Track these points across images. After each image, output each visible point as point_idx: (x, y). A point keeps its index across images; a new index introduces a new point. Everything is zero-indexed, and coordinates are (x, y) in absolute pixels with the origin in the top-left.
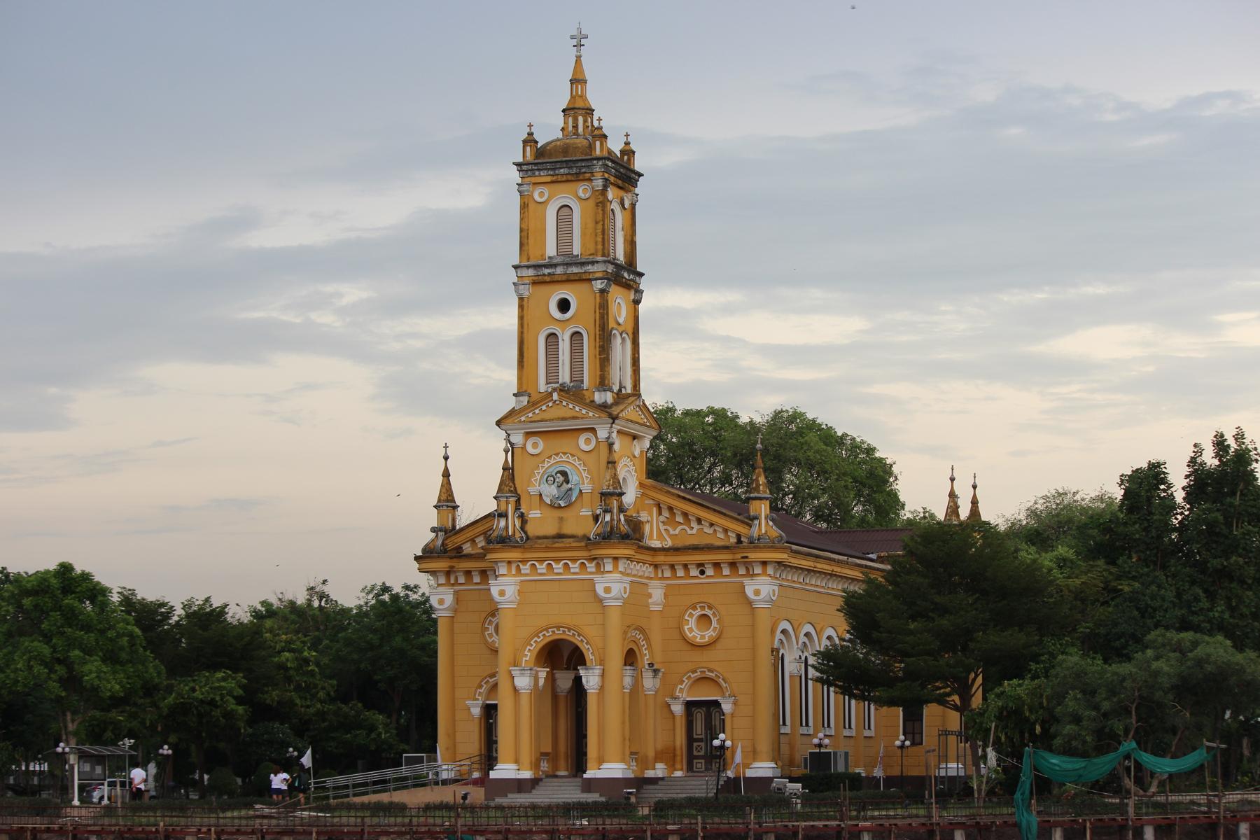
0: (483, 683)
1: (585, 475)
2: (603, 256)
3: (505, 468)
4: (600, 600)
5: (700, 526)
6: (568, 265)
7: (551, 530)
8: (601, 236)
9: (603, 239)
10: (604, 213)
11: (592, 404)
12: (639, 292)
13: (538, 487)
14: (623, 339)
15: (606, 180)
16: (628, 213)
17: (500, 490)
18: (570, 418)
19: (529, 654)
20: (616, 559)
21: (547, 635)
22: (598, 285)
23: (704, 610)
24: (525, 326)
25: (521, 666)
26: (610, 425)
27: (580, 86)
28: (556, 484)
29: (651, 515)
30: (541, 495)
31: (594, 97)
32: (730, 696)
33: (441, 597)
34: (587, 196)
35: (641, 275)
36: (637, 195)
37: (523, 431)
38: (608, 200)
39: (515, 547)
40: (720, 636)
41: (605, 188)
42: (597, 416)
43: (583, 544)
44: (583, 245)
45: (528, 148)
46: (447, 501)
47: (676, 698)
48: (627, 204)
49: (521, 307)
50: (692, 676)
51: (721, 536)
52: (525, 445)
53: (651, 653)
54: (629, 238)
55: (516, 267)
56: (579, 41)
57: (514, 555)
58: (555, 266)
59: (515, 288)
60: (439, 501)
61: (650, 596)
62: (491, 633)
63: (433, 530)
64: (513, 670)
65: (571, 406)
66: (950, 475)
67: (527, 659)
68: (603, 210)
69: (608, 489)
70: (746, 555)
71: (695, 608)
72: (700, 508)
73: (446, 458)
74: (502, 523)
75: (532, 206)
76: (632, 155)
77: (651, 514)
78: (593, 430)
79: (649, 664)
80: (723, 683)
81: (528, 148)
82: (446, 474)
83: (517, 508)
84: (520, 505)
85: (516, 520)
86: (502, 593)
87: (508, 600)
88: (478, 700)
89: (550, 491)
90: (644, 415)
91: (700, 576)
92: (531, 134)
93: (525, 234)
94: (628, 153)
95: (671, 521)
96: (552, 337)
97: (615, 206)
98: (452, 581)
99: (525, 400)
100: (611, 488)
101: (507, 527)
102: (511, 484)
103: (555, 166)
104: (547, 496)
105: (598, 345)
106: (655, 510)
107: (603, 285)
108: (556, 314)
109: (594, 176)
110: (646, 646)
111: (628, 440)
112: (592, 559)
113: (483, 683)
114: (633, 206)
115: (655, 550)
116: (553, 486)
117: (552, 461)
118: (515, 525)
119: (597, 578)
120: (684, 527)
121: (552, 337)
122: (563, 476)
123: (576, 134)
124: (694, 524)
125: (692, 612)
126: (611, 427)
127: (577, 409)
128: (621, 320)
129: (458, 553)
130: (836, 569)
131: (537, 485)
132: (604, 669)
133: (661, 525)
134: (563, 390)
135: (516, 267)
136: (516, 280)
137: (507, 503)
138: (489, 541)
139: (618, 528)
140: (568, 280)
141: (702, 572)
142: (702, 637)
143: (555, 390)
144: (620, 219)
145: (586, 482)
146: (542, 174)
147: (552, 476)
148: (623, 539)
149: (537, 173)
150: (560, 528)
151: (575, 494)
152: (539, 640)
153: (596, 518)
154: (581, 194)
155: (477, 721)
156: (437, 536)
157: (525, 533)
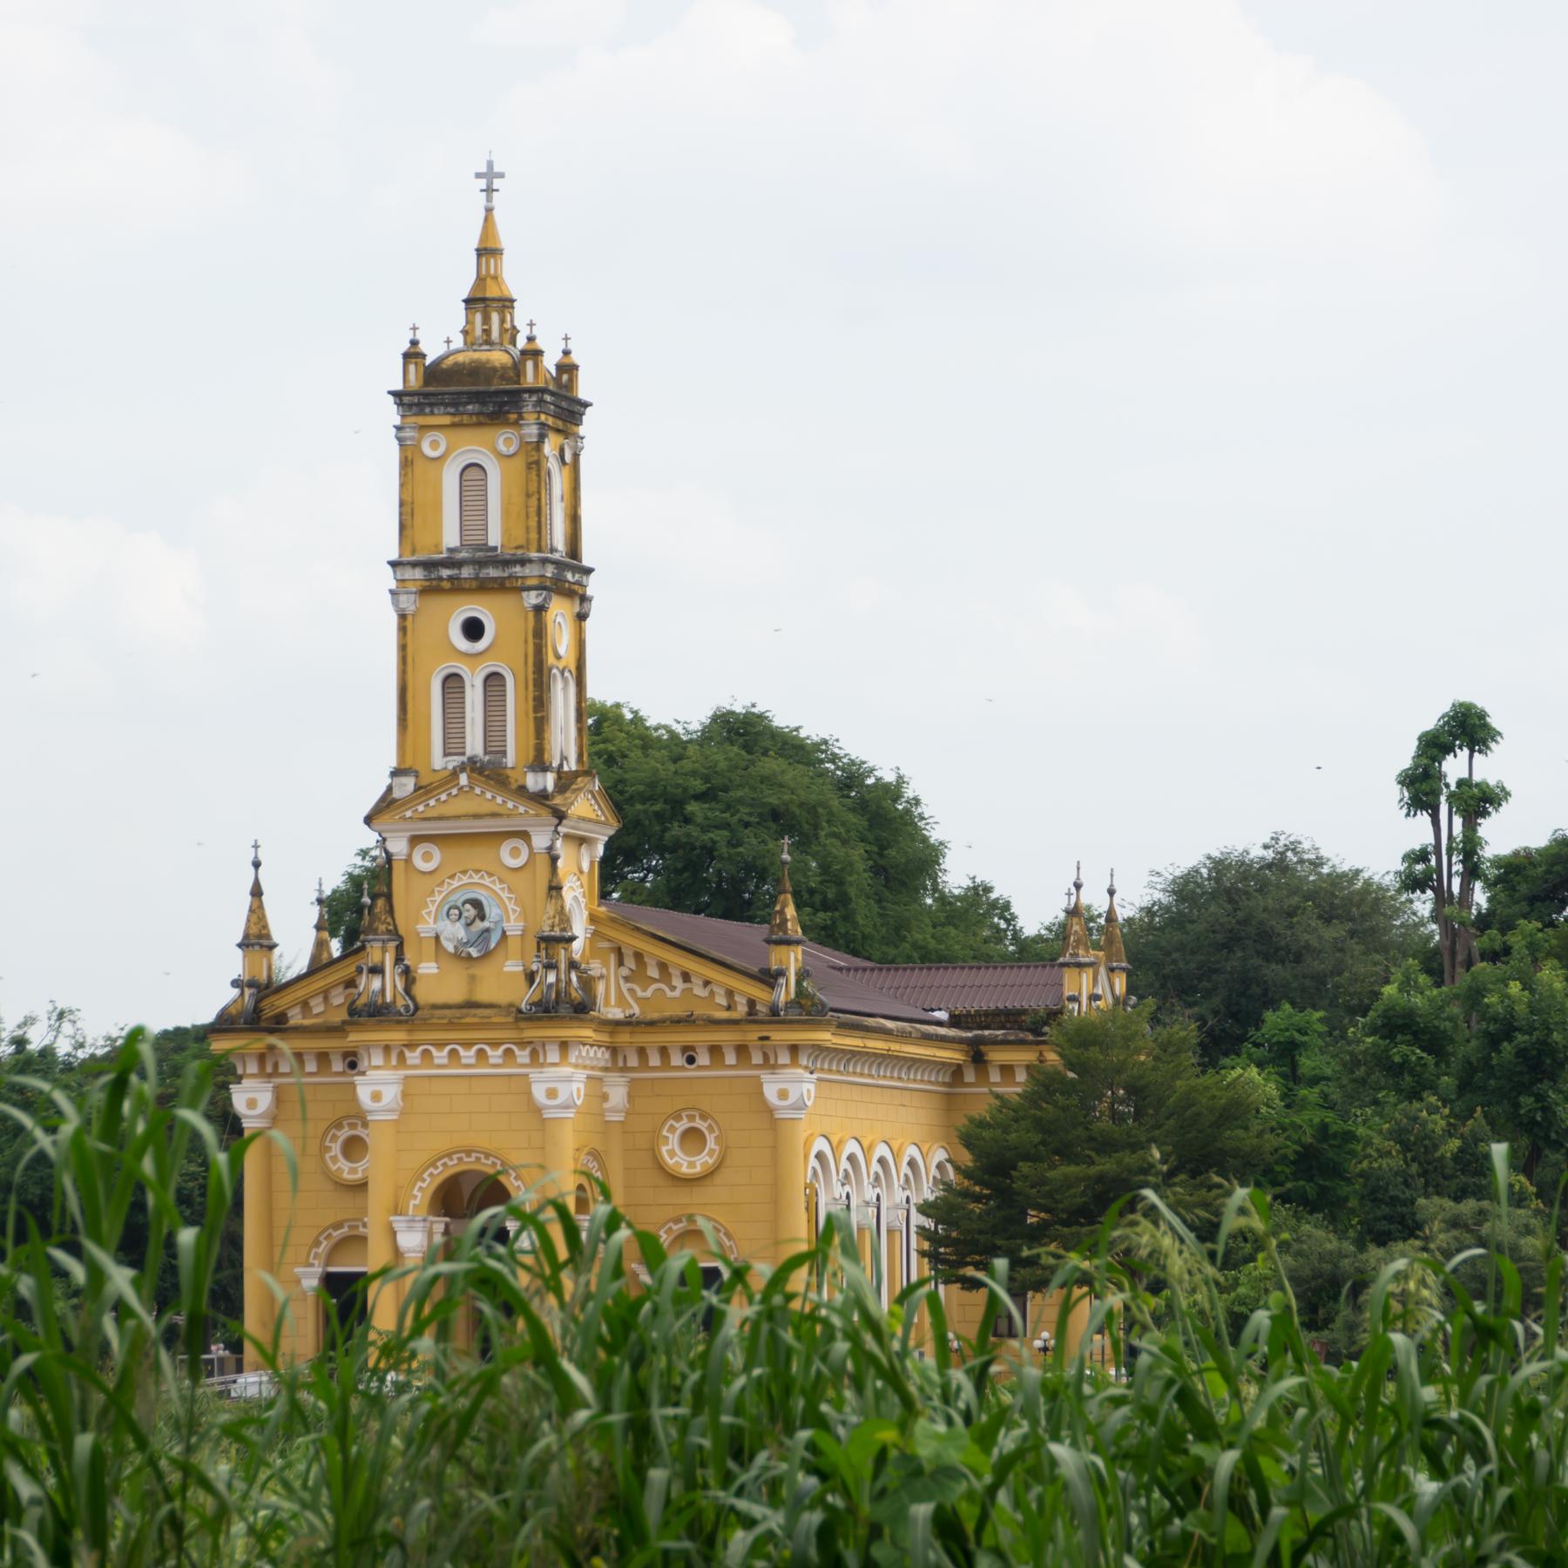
0: (321, 1238)
1: (511, 906)
2: (539, 550)
4: (537, 1110)
5: (688, 985)
6: (480, 564)
9: (539, 522)
10: (539, 476)
12: (584, 599)
13: (432, 925)
14: (565, 688)
15: (542, 425)
18: (487, 815)
19: (419, 1195)
20: (564, 1046)
22: (532, 598)
24: (409, 661)
25: (406, 1215)
27: (492, 261)
29: (608, 970)
30: (437, 938)
31: (514, 277)
33: (251, 1095)
34: (512, 450)
35: (589, 571)
37: (408, 834)
39: (399, 1022)
40: (721, 1162)
42: (531, 812)
43: (510, 1019)
44: (506, 531)
45: (412, 368)
46: (257, 940)
48: (568, 457)
49: (403, 630)
50: (675, 1227)
51: (722, 1000)
55: (394, 564)
57: (397, 1036)
58: (458, 564)
59: (393, 599)
60: (246, 936)
61: (605, 1097)
62: (336, 1156)
63: (236, 983)
65: (489, 795)
66: (1073, 879)
67: (417, 1202)
68: (539, 476)
71: (678, 1118)
72: (721, 969)
73: (257, 865)
74: (376, 984)
75: (419, 465)
77: (605, 964)
78: (524, 836)
81: (412, 368)
82: (257, 892)
83: (399, 959)
84: (402, 954)
85: (397, 978)
86: (376, 1097)
88: (312, 1265)
89: (453, 932)
92: (414, 343)
93: (407, 509)
94: (568, 369)
95: (638, 976)
96: (453, 683)
97: (553, 464)
98: (269, 1069)
101: (383, 990)
102: (389, 920)
103: (455, 403)
104: (448, 939)
105: (531, 696)
106: (613, 959)
108: (462, 643)
109: (522, 419)
112: (522, 1044)
113: (321, 1238)
114: (576, 456)
115: (617, 1023)
116: (458, 924)
117: (456, 883)
118: (395, 986)
119: (534, 1074)
120: (662, 986)
121: (453, 683)
123: (488, 342)
124: (677, 981)
127: (499, 800)
129: (279, 1024)
130: (895, 1047)
131: (431, 921)
133: (622, 982)
134: (473, 766)
135: (394, 564)
136: (393, 585)
137: (384, 950)
139: (567, 993)
140: (484, 587)
141: (691, 1060)
142: (691, 1165)
144: (559, 483)
145: (512, 917)
146: (436, 411)
147: (457, 908)
148: (576, 1012)
149: (427, 410)
151: (495, 938)
153: (530, 977)
154: (502, 448)
155: (311, 1302)
156: (242, 994)
157: (412, 998)
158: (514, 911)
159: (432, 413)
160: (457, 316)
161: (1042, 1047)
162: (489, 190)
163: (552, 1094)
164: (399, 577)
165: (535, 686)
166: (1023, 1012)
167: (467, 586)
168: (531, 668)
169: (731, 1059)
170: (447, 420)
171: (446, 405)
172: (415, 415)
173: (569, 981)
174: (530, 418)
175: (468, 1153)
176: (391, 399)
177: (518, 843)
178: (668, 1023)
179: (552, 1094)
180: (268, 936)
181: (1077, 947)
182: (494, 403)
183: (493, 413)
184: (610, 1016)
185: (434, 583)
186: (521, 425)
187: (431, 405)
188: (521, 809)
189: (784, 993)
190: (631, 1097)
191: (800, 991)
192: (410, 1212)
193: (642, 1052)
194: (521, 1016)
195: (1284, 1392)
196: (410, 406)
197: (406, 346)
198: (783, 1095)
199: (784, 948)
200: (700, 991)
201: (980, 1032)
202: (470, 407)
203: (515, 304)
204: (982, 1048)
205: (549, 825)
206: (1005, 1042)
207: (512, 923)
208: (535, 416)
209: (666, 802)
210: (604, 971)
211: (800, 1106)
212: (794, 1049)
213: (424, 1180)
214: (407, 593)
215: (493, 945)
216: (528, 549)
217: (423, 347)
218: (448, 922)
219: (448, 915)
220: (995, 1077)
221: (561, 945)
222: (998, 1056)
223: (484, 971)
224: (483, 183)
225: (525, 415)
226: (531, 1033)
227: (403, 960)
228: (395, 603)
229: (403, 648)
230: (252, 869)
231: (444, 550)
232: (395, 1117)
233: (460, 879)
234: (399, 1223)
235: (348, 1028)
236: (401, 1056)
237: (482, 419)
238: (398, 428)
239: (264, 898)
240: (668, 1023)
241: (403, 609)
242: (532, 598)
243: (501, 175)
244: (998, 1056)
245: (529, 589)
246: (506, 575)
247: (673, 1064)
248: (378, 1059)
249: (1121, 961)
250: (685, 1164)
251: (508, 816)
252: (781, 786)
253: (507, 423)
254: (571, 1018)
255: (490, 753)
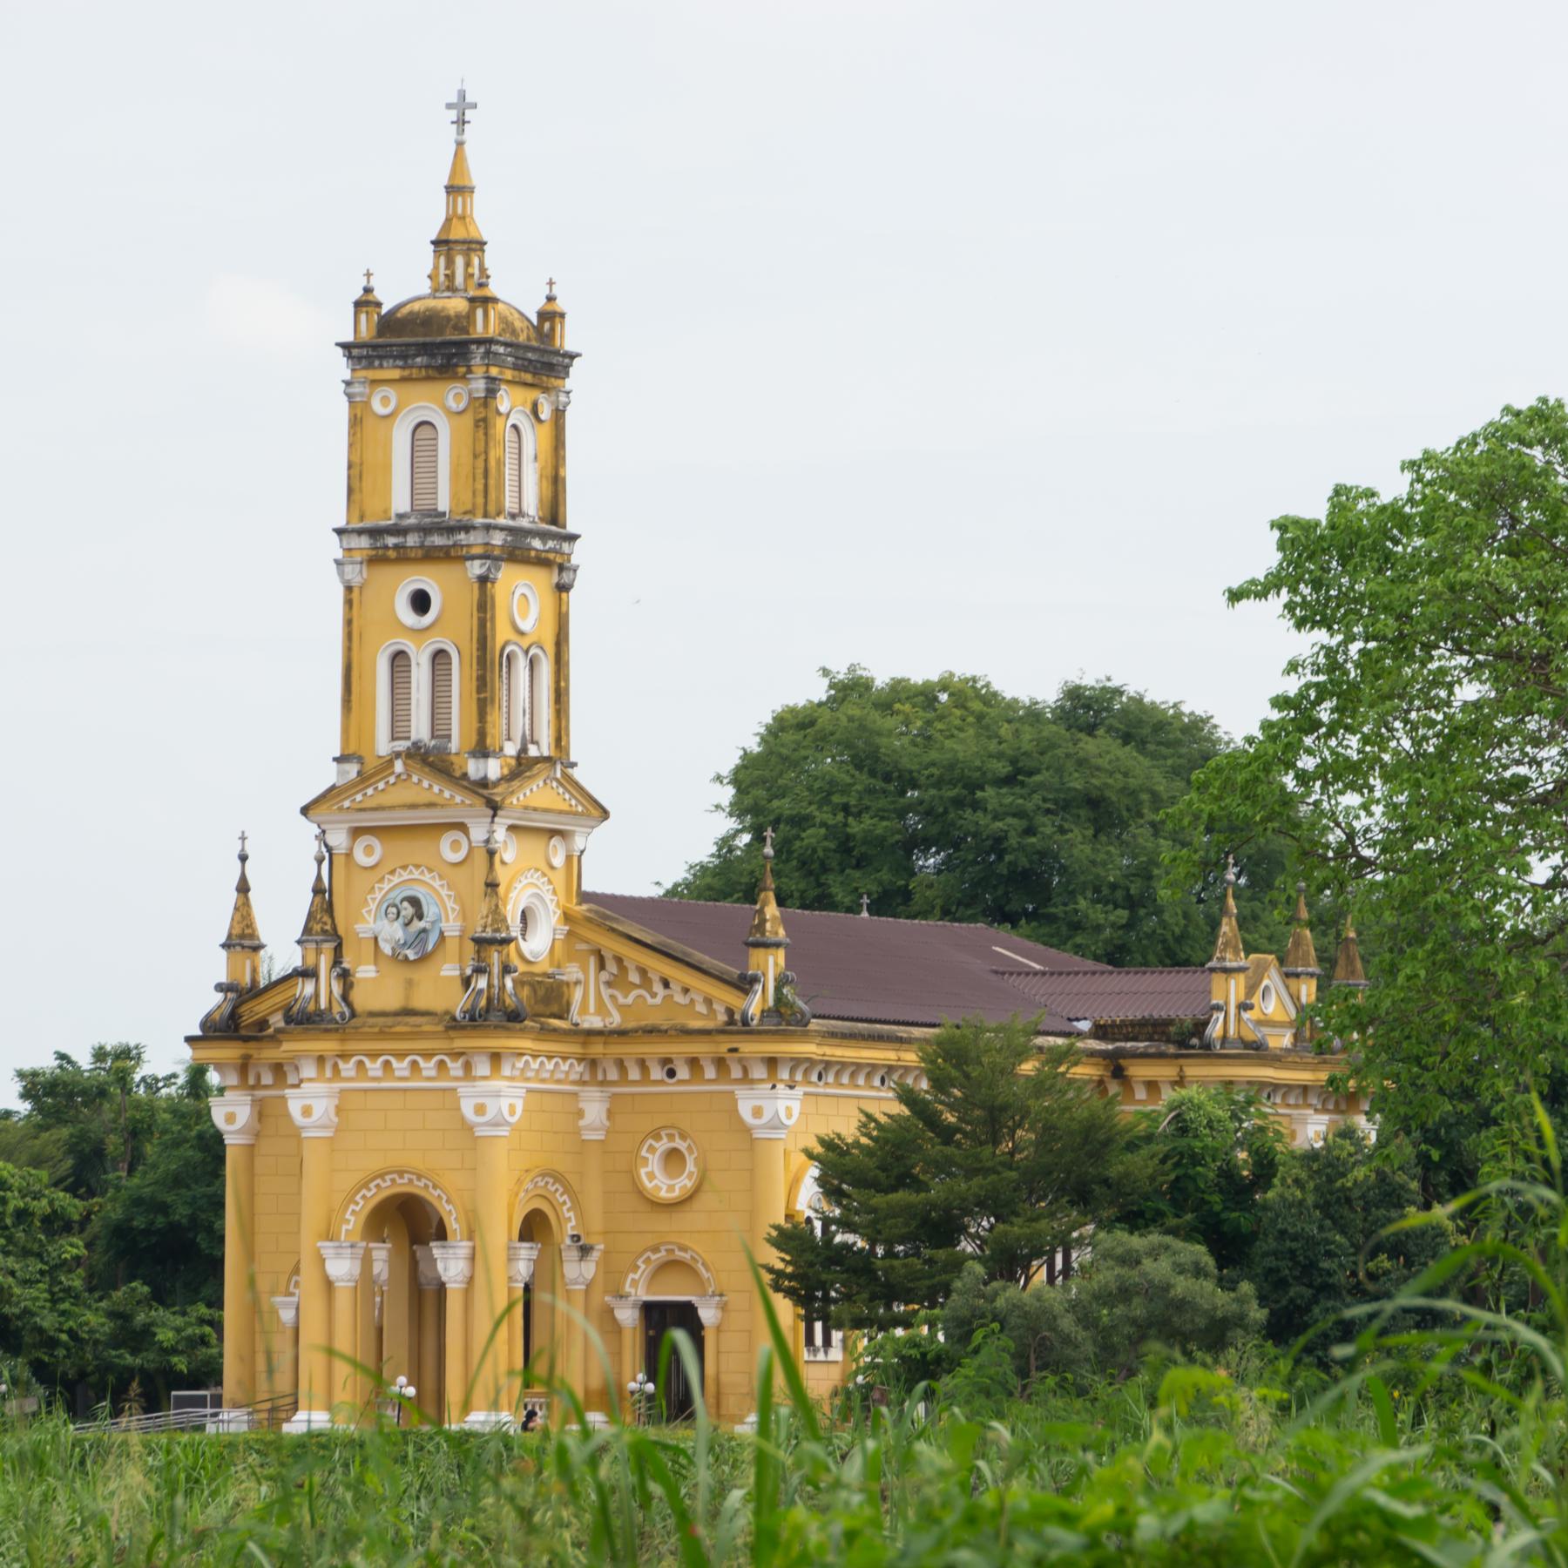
1: (450, 904)
2: (486, 515)
3: (318, 890)
4: (468, 1128)
5: (667, 992)
6: (425, 530)
7: (390, 999)
8: (483, 481)
9: (486, 486)
11: (461, 781)
13: (372, 925)
14: (532, 664)
15: (491, 380)
16: (546, 431)
17: (307, 930)
20: (496, 1058)
21: (383, 1185)
22: (476, 568)
23: (674, 1141)
25: (338, 1240)
26: (489, 820)
27: (460, 199)
28: (401, 920)
29: (586, 972)
30: (376, 939)
31: (485, 218)
32: (713, 1295)
34: (462, 406)
35: (573, 538)
36: (568, 393)
37: (347, 826)
38: (498, 413)
39: (327, 1031)
41: (491, 393)
42: (468, 802)
43: (440, 1028)
44: (454, 496)
45: (363, 317)
46: (242, 940)
47: (621, 1297)
48: (545, 413)
49: (349, 603)
50: (653, 1257)
51: (701, 1008)
52: (351, 849)
53: (581, 1216)
54: (549, 472)
55: (340, 532)
56: (461, 110)
57: (328, 1046)
60: (230, 936)
61: (580, 1114)
63: (220, 987)
64: (324, 1247)
65: (426, 784)
67: (350, 1227)
68: (486, 434)
69: (484, 931)
70: (735, 1045)
71: (658, 1137)
73: (243, 858)
74: (309, 988)
75: (369, 423)
76: (557, 320)
77: (585, 971)
78: (462, 827)
79: (573, 1236)
80: (704, 1271)
81: (363, 317)
82: (243, 888)
83: (337, 961)
86: (307, 1111)
87: (318, 1123)
89: (392, 933)
90: (569, 792)
91: (667, 1079)
92: (368, 290)
93: (355, 471)
94: (550, 316)
96: (399, 659)
98: (251, 1081)
99: (352, 770)
100: (489, 929)
103: (403, 355)
104: (386, 940)
105: (475, 675)
106: (592, 962)
107: (484, 569)
108: (407, 616)
110: (569, 1205)
111: (534, 845)
114: (559, 414)
115: (591, 1033)
117: (396, 880)
118: (331, 992)
119: (464, 1088)
120: (642, 992)
121: (399, 659)
122: (413, 906)
124: (658, 987)
125: (654, 1143)
126: (492, 822)
128: (525, 625)
131: (371, 919)
132: (474, 1248)
133: (602, 987)
135: (340, 532)
136: (339, 554)
137: (318, 952)
138: (289, 1019)
140: (430, 556)
141: (671, 1073)
142: (671, 1188)
143: (398, 755)
145: (451, 917)
147: (395, 906)
148: (509, 1020)
149: (377, 363)
150: (407, 997)
152: (358, 1208)
153: (466, 982)
158: (453, 910)
159: (381, 366)
160: (425, 258)
161: (1182, 1061)
162: (461, 122)
163: (480, 1109)
164: (345, 546)
165: (478, 664)
166: (1169, 1022)
167: (413, 555)
168: (475, 646)
169: (710, 1072)
170: (396, 374)
171: (395, 358)
172: (365, 368)
173: (503, 987)
174: (479, 371)
175: (401, 1173)
176: (340, 351)
177: (457, 835)
178: (640, 1033)
179: (480, 1109)
180: (253, 936)
181: (1224, 950)
182: (443, 355)
183: (442, 366)
184: (586, 1025)
185: (380, 552)
186: (469, 379)
187: (381, 358)
188: (458, 799)
189: (755, 1005)
190: (610, 1114)
191: (779, 998)
192: (343, 1238)
193: (621, 1064)
194: (453, 1025)
195: (934, 1448)
196: (360, 358)
197: (358, 293)
198: (757, 1112)
199: (760, 952)
200: (680, 998)
201: (1122, 1044)
202: (419, 360)
203: (486, 247)
204: (1122, 1062)
205: (485, 816)
206: (1144, 1055)
207: (451, 923)
208: (484, 369)
209: (964, 787)
210: (581, 976)
211: (776, 1125)
212: (772, 1063)
213: (357, 1204)
214: (352, 563)
215: (430, 947)
216: (474, 515)
217: (378, 295)
218: (386, 921)
219: (386, 914)
220: (1141, 1094)
221: (493, 948)
222: (1139, 1071)
223: (422, 975)
224: (453, 115)
225: (474, 369)
226: (460, 1043)
227: (341, 963)
228: (341, 574)
229: (349, 623)
230: (239, 863)
231: (393, 515)
232: (330, 1134)
233: (400, 875)
234: (327, 1249)
235: (280, 1036)
236: (335, 1067)
237: (431, 372)
238: (348, 383)
239: (251, 894)
240: (640, 1033)
241: (349, 581)
242: (476, 568)
243: (474, 106)
244: (1139, 1071)
245: (473, 558)
246: (451, 543)
247: (652, 1078)
248: (308, 1070)
249: (1309, 965)
250: (665, 1188)
251: (442, 806)
252: (1098, 769)
253: (455, 377)
254: (504, 1028)
255: (438, 737)
